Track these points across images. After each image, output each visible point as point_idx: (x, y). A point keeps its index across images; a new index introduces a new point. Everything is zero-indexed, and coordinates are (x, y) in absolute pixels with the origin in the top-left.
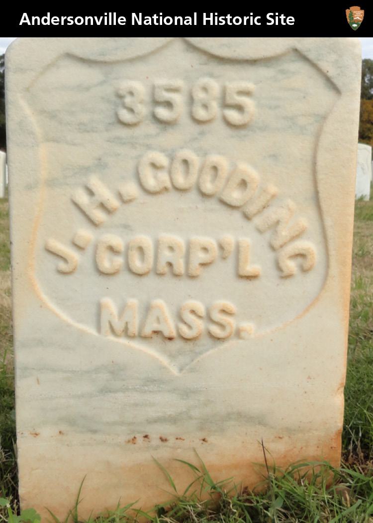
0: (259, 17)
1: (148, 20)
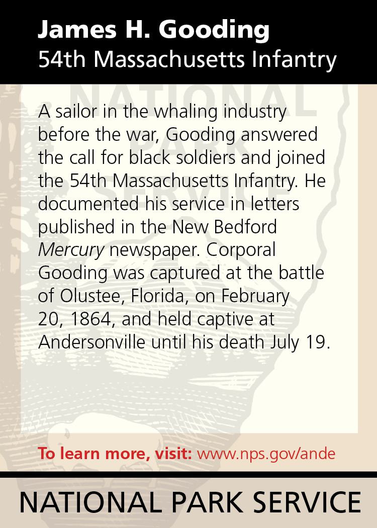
0: (280, 50)
1: (56, 31)
